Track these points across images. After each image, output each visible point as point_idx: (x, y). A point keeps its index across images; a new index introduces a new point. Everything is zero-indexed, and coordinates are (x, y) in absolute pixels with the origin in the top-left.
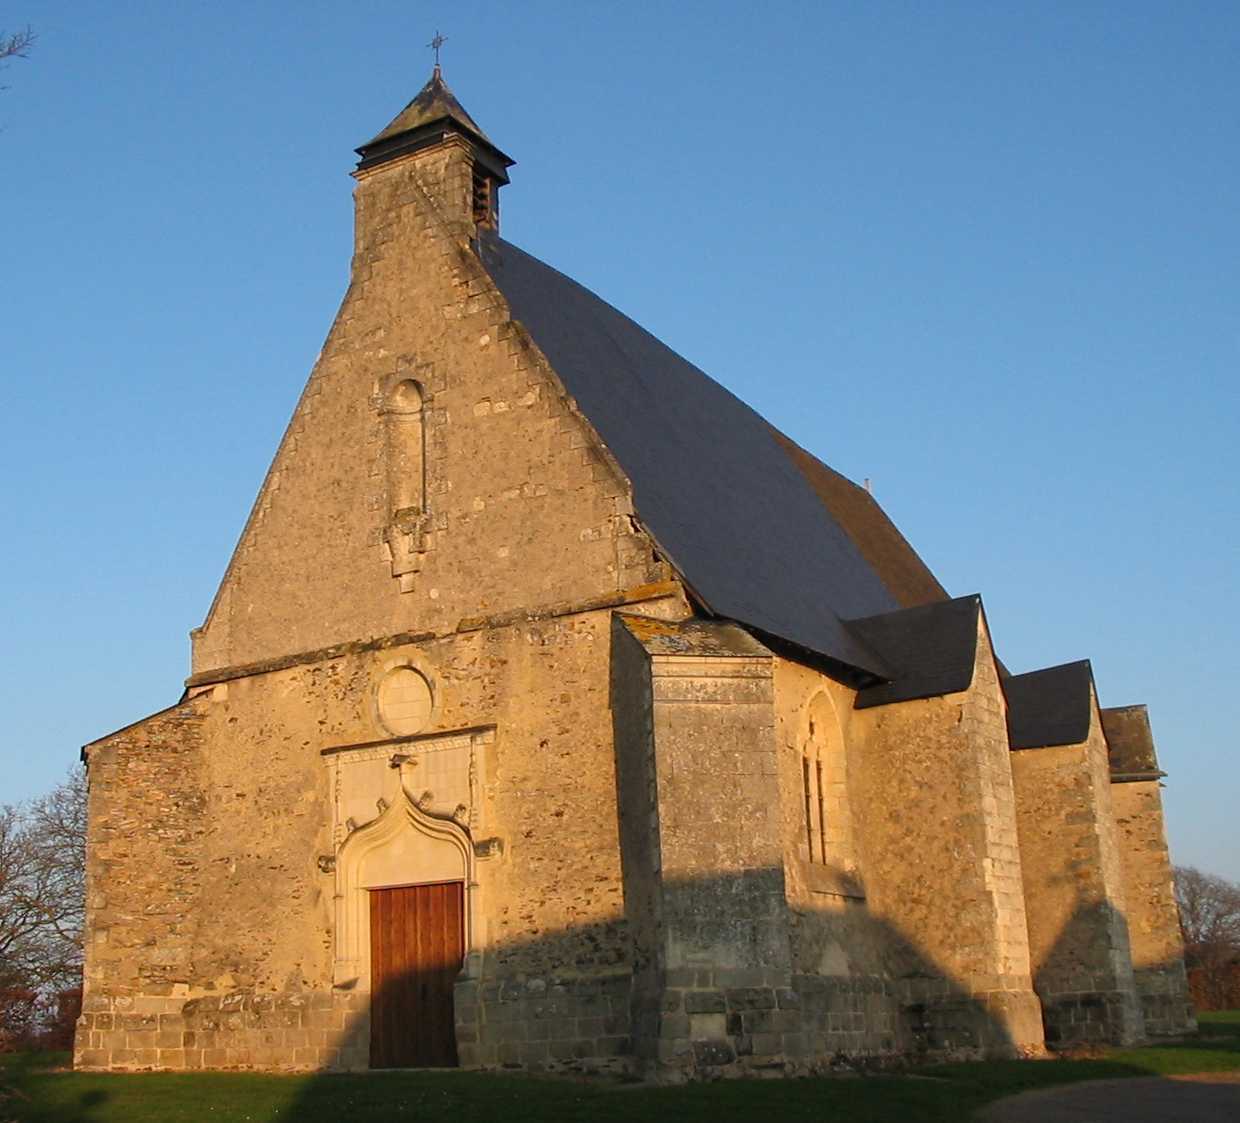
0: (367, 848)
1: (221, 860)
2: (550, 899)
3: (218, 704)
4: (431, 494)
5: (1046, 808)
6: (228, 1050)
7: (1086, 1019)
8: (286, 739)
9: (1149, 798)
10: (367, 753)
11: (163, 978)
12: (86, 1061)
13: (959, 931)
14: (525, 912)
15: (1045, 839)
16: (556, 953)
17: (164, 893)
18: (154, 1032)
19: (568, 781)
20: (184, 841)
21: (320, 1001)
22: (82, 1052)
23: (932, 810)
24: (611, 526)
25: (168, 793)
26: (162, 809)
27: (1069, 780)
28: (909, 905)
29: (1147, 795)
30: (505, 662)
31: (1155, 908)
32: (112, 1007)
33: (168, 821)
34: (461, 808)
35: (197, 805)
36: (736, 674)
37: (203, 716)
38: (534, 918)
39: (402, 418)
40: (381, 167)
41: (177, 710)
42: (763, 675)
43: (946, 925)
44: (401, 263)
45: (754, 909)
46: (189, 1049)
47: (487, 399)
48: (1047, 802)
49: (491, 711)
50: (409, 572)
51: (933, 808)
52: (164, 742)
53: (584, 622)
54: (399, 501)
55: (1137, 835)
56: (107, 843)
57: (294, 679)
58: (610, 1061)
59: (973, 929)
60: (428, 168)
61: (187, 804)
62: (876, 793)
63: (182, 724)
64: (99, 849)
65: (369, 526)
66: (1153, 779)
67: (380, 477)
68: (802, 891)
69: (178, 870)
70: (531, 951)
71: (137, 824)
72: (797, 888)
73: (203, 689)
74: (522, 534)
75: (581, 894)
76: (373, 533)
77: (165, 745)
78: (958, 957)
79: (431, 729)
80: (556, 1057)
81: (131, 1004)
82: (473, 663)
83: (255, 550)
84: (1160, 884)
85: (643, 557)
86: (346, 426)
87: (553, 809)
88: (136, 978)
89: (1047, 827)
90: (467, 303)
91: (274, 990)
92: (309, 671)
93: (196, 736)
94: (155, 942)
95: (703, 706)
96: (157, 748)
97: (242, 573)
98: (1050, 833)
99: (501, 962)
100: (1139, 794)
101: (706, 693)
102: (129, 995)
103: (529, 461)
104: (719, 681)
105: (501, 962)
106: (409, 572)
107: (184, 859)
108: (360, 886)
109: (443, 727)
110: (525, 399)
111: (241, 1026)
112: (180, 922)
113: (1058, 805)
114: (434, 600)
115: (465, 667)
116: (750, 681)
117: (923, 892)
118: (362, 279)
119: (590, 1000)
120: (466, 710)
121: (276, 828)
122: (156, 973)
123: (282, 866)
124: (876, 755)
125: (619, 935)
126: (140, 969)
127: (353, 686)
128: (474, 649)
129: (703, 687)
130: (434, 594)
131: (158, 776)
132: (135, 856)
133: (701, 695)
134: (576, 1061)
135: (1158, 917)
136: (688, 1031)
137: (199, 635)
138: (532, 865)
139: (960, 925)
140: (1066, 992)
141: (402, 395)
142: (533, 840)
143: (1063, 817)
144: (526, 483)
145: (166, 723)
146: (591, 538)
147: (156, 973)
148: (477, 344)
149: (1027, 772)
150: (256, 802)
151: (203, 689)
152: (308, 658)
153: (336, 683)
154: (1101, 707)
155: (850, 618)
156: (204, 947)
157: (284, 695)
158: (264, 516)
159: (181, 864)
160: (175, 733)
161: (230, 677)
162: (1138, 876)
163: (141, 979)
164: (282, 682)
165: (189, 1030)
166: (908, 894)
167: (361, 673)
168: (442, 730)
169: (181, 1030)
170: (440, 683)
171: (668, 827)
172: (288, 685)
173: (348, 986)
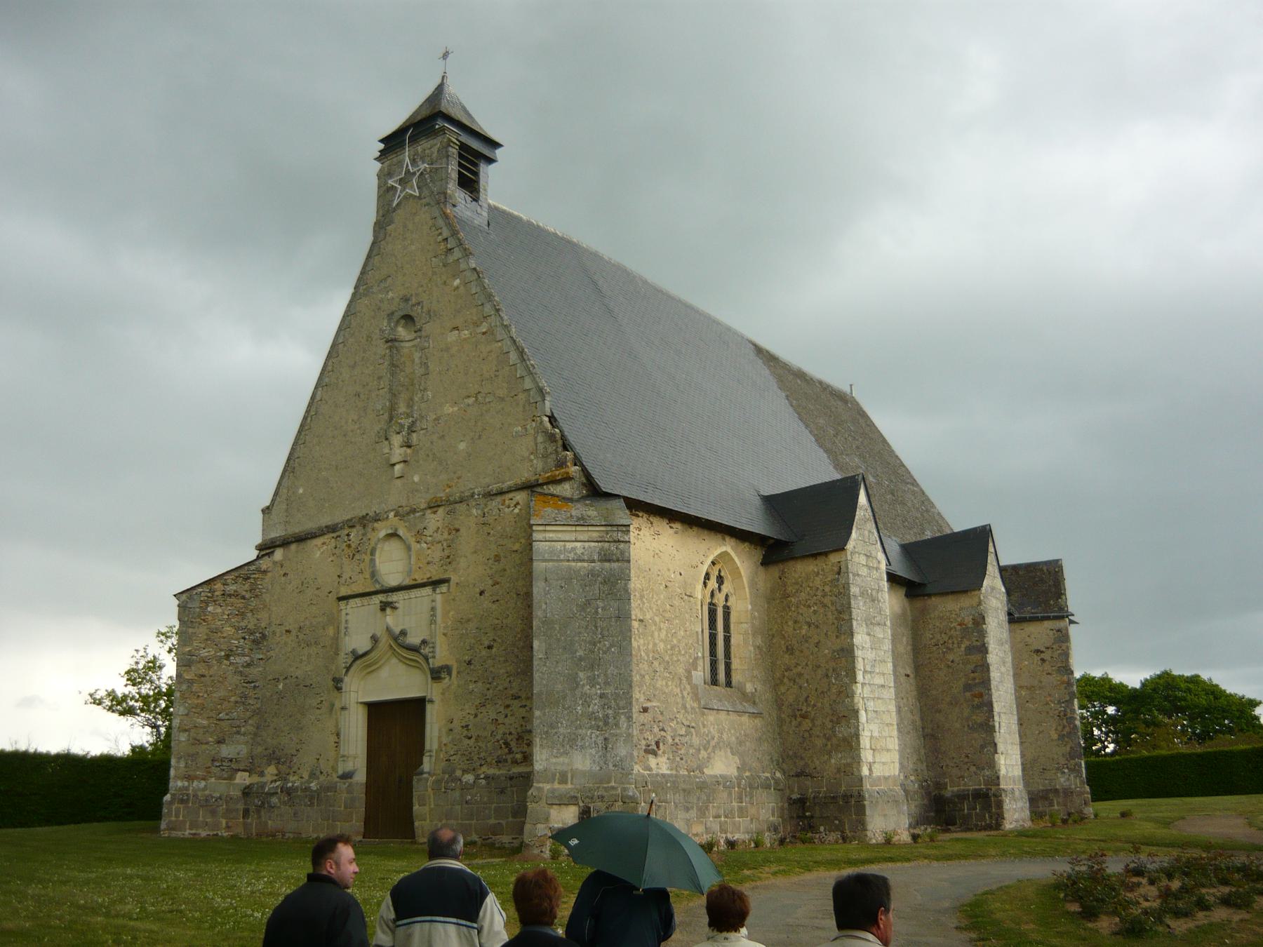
0: (365, 672)
1: (274, 679)
2: (481, 713)
3: (276, 562)
4: (417, 402)
5: (950, 641)
6: (270, 822)
7: (976, 809)
8: (318, 589)
9: (1059, 633)
10: (365, 600)
11: (230, 767)
12: (170, 829)
13: (834, 741)
14: (464, 724)
15: (949, 667)
16: (482, 755)
17: (232, 704)
18: (221, 808)
19: (497, 622)
20: (249, 665)
21: (332, 788)
22: (167, 821)
23: (817, 645)
24: (534, 424)
25: (237, 629)
26: (233, 641)
27: (969, 621)
28: (799, 719)
29: (1058, 631)
30: (458, 530)
31: (1062, 720)
32: (191, 788)
33: (236, 650)
34: (424, 642)
35: (259, 639)
36: (601, 539)
37: (265, 572)
38: (470, 727)
39: (402, 344)
40: (396, 153)
41: (246, 567)
42: (622, 539)
43: (825, 735)
44: (405, 226)
45: (606, 723)
46: (246, 820)
47: (456, 328)
48: (951, 637)
49: (447, 568)
50: (401, 462)
51: (817, 643)
52: (235, 591)
53: (511, 499)
54: (399, 407)
55: (1050, 662)
56: (190, 666)
57: (324, 544)
58: (513, 839)
59: (845, 739)
60: (427, 151)
61: (252, 637)
62: (777, 630)
63: (249, 578)
64: (184, 671)
65: (377, 428)
66: (1062, 618)
67: (386, 390)
68: (693, 708)
69: (243, 687)
70: (467, 753)
71: (214, 652)
72: (688, 706)
73: (268, 551)
74: (475, 432)
75: (502, 709)
76: (379, 433)
77: (235, 595)
78: (833, 761)
79: (407, 582)
80: (478, 835)
81: (205, 786)
82: (437, 531)
83: (305, 447)
84: (1066, 701)
85: (554, 448)
86: (365, 351)
87: (486, 643)
88: (209, 767)
89: (951, 657)
90: (446, 255)
91: (302, 778)
92: (333, 537)
93: (260, 587)
94: (224, 740)
95: (574, 564)
96: (230, 595)
97: (296, 465)
98: (952, 662)
99: (446, 760)
100: (1052, 630)
101: (576, 554)
102: (204, 779)
103: (481, 375)
104: (587, 545)
105: (446, 760)
106: (401, 462)
107: (248, 679)
108: (360, 701)
109: (415, 580)
110: (481, 327)
111: (279, 805)
112: (243, 726)
113: (960, 639)
114: (416, 483)
115: (431, 534)
116: (612, 544)
117: (810, 709)
118: (380, 239)
119: (502, 791)
120: (430, 567)
121: (309, 656)
122: (224, 764)
123: (311, 685)
124: (778, 601)
125: (525, 742)
126: (212, 760)
127: (359, 549)
128: (438, 521)
129: (574, 549)
130: (416, 479)
131: (230, 617)
132: (211, 676)
133: (571, 556)
134: (491, 838)
135: (1064, 727)
136: (547, 819)
137: (267, 511)
138: (471, 687)
139: (835, 736)
140: (962, 788)
141: (402, 327)
142: (472, 667)
143: (963, 649)
144: (479, 392)
145: (237, 577)
146: (521, 434)
147: (224, 764)
148: (452, 286)
149: (937, 613)
150: (297, 636)
151: (268, 551)
152: (332, 529)
153: (349, 546)
154: (1001, 564)
155: (766, 494)
156: (260, 744)
157: (318, 555)
158: (311, 420)
159: (247, 683)
160: (244, 585)
161: (285, 543)
162: (1050, 695)
163: (213, 768)
164: (317, 546)
165: (246, 807)
166: (798, 710)
167: (364, 539)
168: (414, 583)
169: (241, 806)
170: (415, 546)
171: (541, 658)
172: (318, 550)
173: (347, 776)
